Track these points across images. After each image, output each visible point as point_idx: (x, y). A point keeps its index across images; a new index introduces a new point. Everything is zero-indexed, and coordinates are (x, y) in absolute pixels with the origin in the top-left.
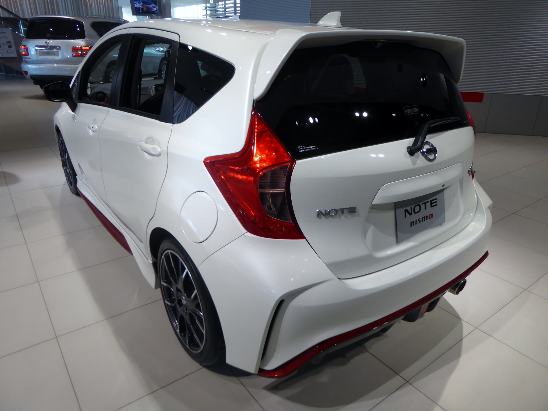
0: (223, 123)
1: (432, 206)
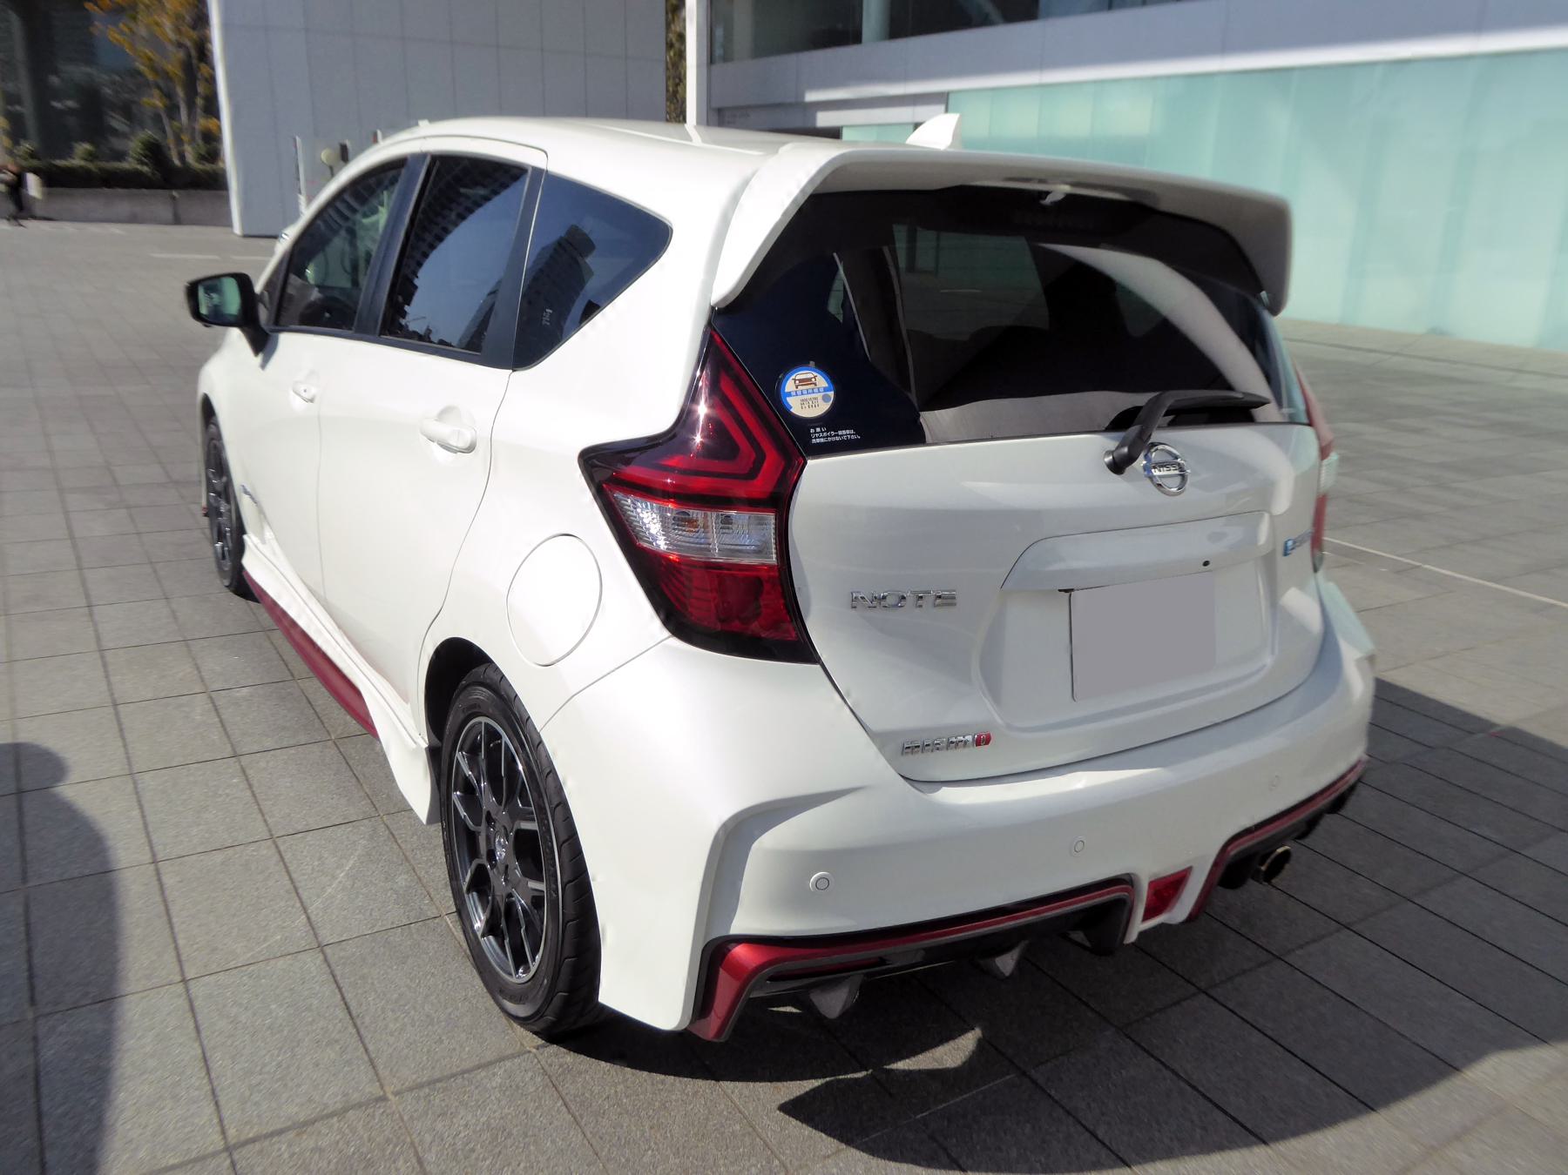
0: (638, 362)
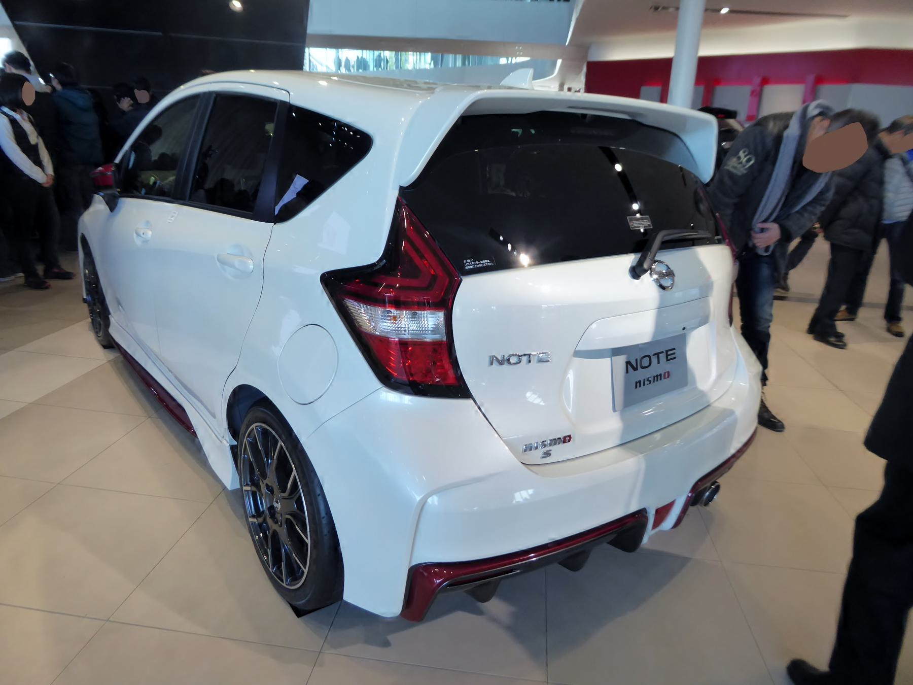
1: (667, 360)
